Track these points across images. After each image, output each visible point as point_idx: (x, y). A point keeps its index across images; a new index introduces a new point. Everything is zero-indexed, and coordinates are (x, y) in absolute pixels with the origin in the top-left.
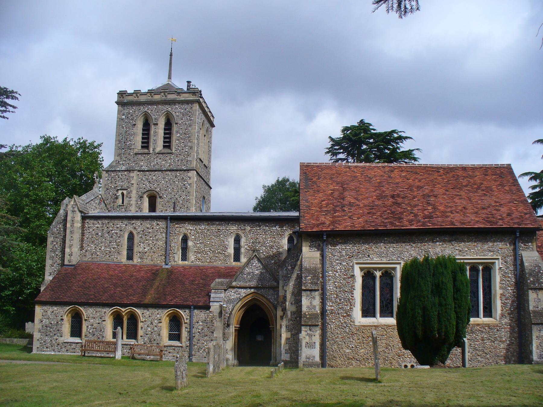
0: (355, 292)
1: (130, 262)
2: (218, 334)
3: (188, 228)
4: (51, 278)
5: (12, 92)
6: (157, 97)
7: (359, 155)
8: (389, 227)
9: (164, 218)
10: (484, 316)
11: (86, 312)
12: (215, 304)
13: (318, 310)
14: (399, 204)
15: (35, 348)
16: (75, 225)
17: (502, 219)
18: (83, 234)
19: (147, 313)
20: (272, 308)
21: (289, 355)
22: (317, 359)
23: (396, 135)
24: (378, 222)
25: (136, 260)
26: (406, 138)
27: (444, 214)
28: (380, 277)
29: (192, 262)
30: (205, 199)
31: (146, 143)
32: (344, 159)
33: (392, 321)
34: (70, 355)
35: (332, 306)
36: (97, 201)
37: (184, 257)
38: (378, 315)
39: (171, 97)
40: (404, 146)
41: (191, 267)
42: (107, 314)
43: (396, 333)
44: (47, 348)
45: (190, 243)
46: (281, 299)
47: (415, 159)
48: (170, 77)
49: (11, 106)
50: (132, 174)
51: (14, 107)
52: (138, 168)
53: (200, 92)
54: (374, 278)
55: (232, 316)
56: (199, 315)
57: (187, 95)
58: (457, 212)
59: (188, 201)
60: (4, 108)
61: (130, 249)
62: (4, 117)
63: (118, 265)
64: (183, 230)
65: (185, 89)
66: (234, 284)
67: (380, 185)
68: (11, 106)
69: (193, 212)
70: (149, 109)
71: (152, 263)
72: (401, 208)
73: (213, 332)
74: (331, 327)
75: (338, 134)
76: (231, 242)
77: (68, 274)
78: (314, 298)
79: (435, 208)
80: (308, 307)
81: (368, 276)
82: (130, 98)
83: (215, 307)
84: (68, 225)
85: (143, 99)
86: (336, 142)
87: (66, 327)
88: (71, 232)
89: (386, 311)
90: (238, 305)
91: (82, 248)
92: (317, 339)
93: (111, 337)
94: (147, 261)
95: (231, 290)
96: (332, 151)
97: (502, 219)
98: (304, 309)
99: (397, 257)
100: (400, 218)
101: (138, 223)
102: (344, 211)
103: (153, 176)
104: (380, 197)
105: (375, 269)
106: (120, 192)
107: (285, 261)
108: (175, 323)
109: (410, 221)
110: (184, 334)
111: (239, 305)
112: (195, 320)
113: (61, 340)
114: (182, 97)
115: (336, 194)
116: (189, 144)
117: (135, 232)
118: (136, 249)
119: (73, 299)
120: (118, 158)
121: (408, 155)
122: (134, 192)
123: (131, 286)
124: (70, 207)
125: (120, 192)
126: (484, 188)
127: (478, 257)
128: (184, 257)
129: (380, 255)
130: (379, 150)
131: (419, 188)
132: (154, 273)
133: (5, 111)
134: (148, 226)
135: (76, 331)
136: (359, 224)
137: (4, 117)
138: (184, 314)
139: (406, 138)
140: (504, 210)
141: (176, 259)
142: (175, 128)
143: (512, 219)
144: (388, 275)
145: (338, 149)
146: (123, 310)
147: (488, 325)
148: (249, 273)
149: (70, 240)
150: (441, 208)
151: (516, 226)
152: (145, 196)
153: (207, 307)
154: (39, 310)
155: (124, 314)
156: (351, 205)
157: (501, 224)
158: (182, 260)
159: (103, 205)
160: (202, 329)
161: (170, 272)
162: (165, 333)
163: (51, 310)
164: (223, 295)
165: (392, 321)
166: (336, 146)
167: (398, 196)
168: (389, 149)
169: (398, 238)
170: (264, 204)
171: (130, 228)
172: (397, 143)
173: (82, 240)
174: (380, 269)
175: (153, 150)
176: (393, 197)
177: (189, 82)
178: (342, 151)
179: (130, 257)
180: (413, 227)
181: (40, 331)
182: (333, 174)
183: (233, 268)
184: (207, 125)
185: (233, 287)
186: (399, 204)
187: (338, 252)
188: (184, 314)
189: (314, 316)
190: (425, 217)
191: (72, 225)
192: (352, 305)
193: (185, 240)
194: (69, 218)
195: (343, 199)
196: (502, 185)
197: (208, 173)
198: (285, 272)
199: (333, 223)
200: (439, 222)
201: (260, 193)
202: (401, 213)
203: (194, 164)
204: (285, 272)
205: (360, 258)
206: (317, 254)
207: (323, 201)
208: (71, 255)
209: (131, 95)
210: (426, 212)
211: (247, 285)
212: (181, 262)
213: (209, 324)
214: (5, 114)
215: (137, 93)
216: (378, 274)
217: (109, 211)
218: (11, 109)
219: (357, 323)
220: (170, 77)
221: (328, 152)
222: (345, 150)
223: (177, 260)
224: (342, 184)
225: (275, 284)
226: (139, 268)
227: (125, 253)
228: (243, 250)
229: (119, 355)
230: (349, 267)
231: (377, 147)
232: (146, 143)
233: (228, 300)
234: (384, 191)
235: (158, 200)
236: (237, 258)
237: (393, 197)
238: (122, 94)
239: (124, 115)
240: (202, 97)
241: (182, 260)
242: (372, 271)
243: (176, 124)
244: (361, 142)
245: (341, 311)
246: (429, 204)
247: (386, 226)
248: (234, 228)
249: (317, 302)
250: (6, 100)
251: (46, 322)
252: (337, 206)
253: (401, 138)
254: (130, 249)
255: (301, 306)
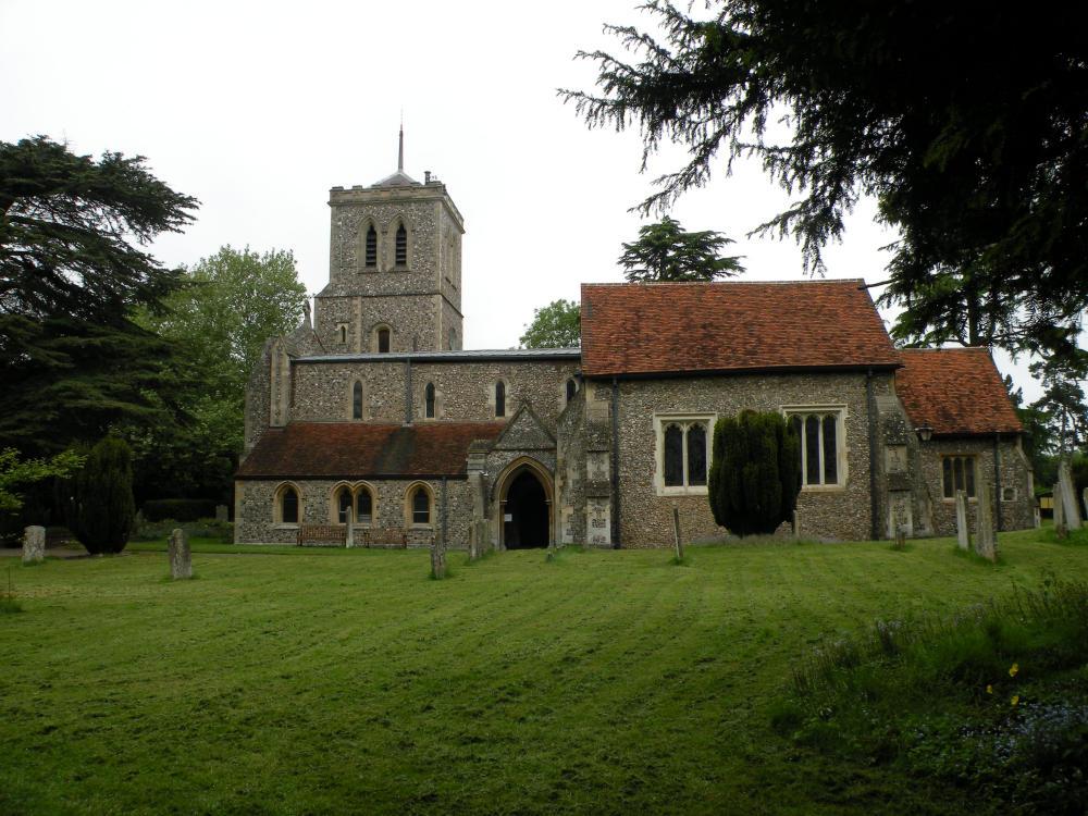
0: (656, 453)
1: (359, 421)
2: (478, 512)
3: (434, 373)
4: (252, 445)
5: (190, 198)
6: (384, 195)
7: (664, 264)
8: (699, 368)
9: (403, 360)
10: (827, 482)
11: (302, 489)
12: (474, 473)
13: (607, 477)
14: (712, 337)
15: (237, 538)
16: (283, 374)
17: (849, 354)
18: (293, 385)
19: (385, 486)
20: (549, 477)
21: (571, 537)
22: (608, 541)
23: (713, 237)
24: (683, 361)
25: (367, 418)
26: (727, 241)
27: (772, 349)
28: (689, 433)
29: (442, 418)
30: (454, 333)
31: (371, 260)
32: (643, 271)
33: (703, 490)
34: (1035, 483)
35: (625, 472)
36: (309, 341)
37: (430, 412)
38: (686, 481)
39: (404, 194)
40: (724, 252)
41: (440, 425)
42: (332, 488)
43: (707, 506)
44: (253, 537)
45: (438, 394)
46: (560, 464)
47: (742, 270)
48: (401, 166)
49: (188, 216)
50: (354, 302)
51: (193, 219)
52: (364, 293)
53: (444, 186)
54: (681, 433)
55: (497, 488)
56: (455, 487)
57: (425, 191)
58: (789, 346)
59: (432, 335)
60: (178, 220)
61: (358, 404)
62: (179, 231)
63: (343, 426)
64: (428, 376)
65: (423, 183)
66: (498, 446)
67: (686, 313)
68: (188, 216)
69: (439, 353)
70: (371, 211)
71: (387, 421)
72: (715, 341)
73: (471, 510)
74: (626, 500)
75: (634, 238)
76: (492, 390)
77: (275, 441)
78: (603, 462)
79: (760, 341)
80: (594, 473)
81: (672, 433)
82: (348, 197)
83: (474, 475)
84: (273, 374)
85: (365, 197)
86: (631, 249)
87: (277, 510)
88: (278, 384)
89: (697, 477)
90: (505, 472)
91: (292, 404)
92: (607, 515)
93: (338, 520)
94: (382, 419)
95: (494, 453)
96: (626, 261)
97: (849, 354)
98: (590, 476)
99: (710, 410)
100: (713, 356)
101: (368, 367)
102: (639, 347)
103: (383, 303)
104: (688, 327)
105: (682, 422)
106: (340, 326)
107: (563, 415)
108: (421, 500)
109: (727, 359)
110: (433, 512)
111: (507, 472)
112: (448, 494)
113: (272, 526)
114: (418, 195)
115: (629, 326)
116: (432, 259)
117: (363, 381)
118: (365, 404)
119: (285, 472)
120: (335, 280)
121: (730, 263)
122: (359, 326)
123: (362, 452)
124: (274, 349)
125: (340, 326)
126: (827, 312)
127: (818, 404)
128: (430, 412)
129: (687, 403)
130: (693, 259)
131: (739, 314)
132: (394, 434)
133: (181, 223)
134: (382, 372)
135: (290, 513)
136: (658, 364)
137: (179, 231)
138: (433, 487)
139: (727, 241)
140: (853, 341)
141: (420, 415)
142: (410, 238)
143: (863, 354)
144: (697, 432)
145: (634, 258)
146: (353, 484)
147: (831, 494)
148: (517, 432)
149: (277, 394)
150: (769, 341)
151: (868, 363)
152: (374, 330)
153: (464, 477)
154: (240, 489)
155: (353, 489)
156: (648, 339)
157: (848, 361)
158: (428, 416)
159: (317, 345)
160: (458, 506)
161: (412, 432)
162: (408, 512)
163: (256, 487)
164: (483, 461)
165: (703, 490)
166: (632, 253)
167: (711, 324)
168: (704, 256)
169: (710, 382)
170: (536, 335)
171: (357, 375)
172: (716, 247)
173: (292, 394)
174: (688, 422)
175: (383, 269)
176: (704, 327)
177: (428, 173)
178: (639, 260)
179: (358, 415)
180: (731, 367)
181: (242, 516)
182: (625, 298)
183: (495, 425)
184: (454, 230)
185: (497, 450)
186: (712, 337)
187: (633, 402)
188: (433, 487)
189: (602, 486)
190: (748, 353)
191: (278, 375)
192: (652, 471)
193: (431, 389)
194: (274, 365)
195: (638, 330)
196: (851, 307)
197: (459, 297)
198: (565, 429)
199: (625, 363)
200: (766, 360)
201: (531, 319)
202: (716, 348)
203: (439, 286)
204: (565, 429)
205: (662, 408)
206: (605, 405)
207: (612, 334)
208: (278, 414)
209: (348, 192)
210: (748, 346)
211: (515, 446)
212: (426, 419)
213: (466, 500)
214: (181, 227)
215: (357, 189)
216: (685, 429)
217: (326, 352)
218: (186, 220)
219: (659, 494)
220: (401, 166)
221: (620, 263)
222: (644, 257)
223: (421, 416)
224: (637, 311)
225: (552, 445)
226: (369, 429)
227: (351, 409)
228: (507, 401)
229: (350, 542)
230: (649, 420)
231: (689, 253)
232: (371, 260)
233: (489, 467)
234: (692, 320)
235: (391, 335)
236: (500, 411)
237: (704, 327)
238: (336, 192)
239: (340, 220)
240: (446, 194)
241: (428, 416)
242: (678, 425)
243: (413, 231)
244: (666, 247)
245: (637, 478)
246: (751, 335)
247: (693, 366)
248: (495, 370)
249: (606, 467)
250: (182, 209)
251: (250, 503)
252: (631, 340)
253: (720, 240)
254: (358, 404)
255: (586, 472)
